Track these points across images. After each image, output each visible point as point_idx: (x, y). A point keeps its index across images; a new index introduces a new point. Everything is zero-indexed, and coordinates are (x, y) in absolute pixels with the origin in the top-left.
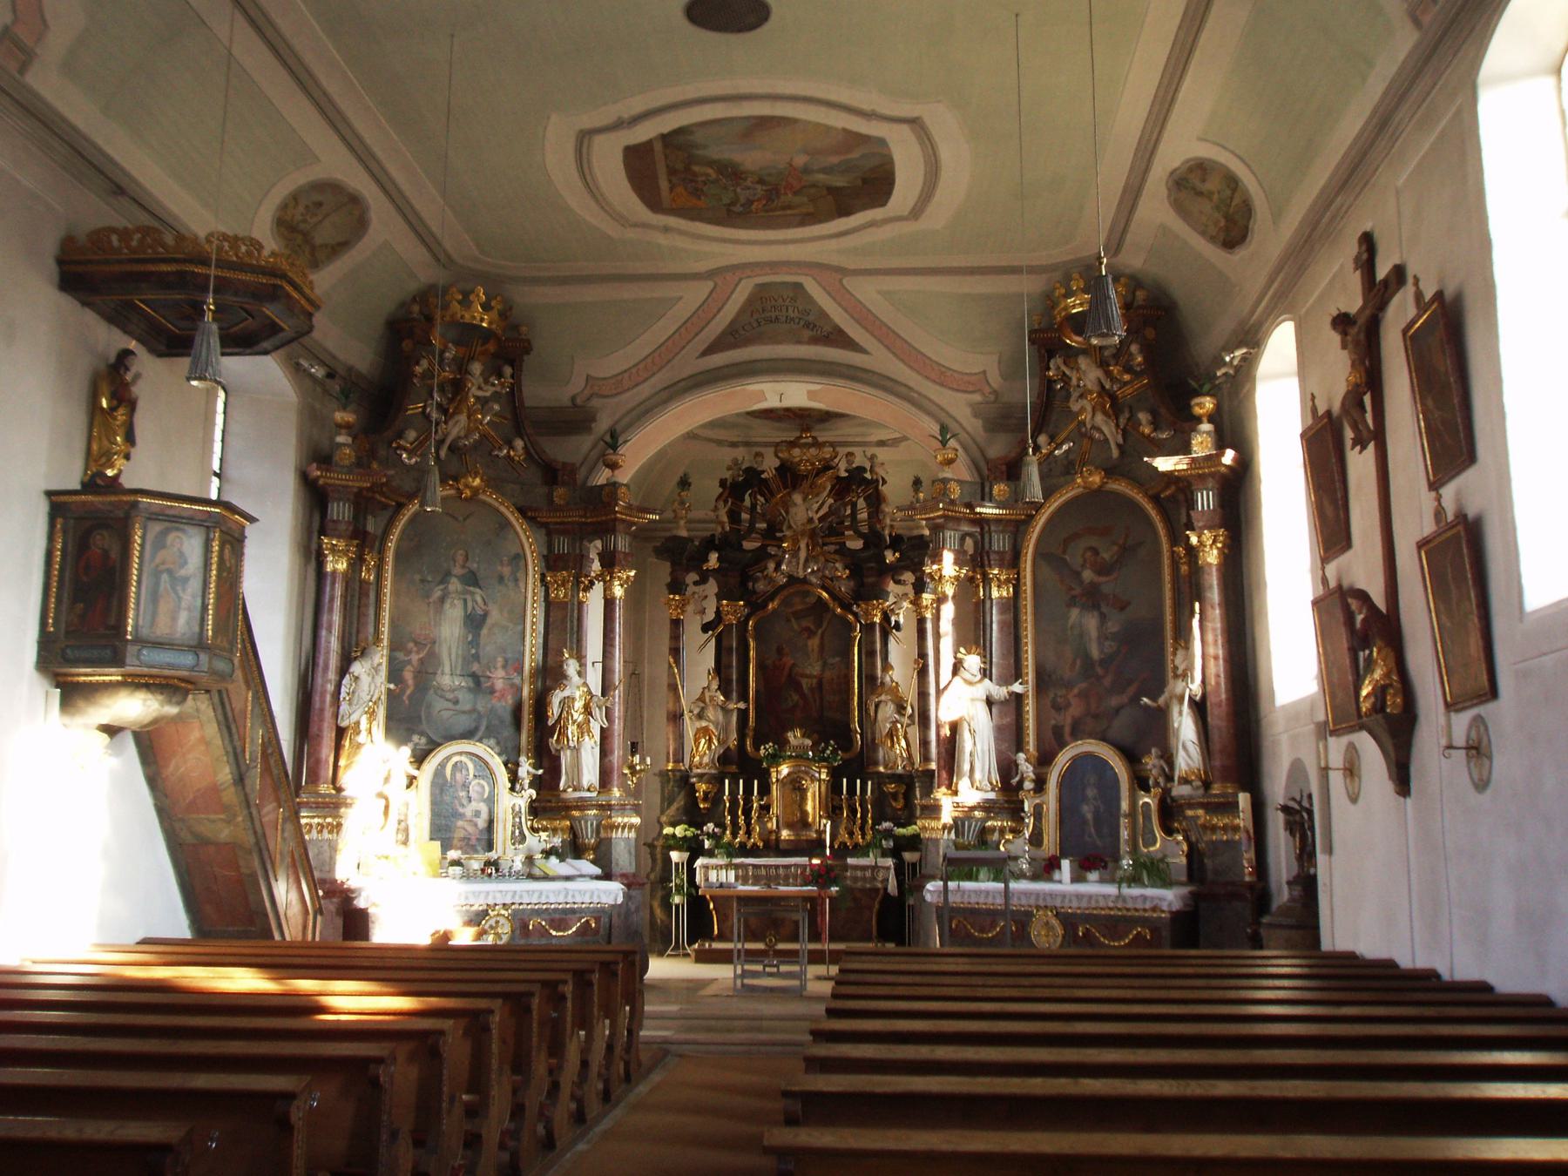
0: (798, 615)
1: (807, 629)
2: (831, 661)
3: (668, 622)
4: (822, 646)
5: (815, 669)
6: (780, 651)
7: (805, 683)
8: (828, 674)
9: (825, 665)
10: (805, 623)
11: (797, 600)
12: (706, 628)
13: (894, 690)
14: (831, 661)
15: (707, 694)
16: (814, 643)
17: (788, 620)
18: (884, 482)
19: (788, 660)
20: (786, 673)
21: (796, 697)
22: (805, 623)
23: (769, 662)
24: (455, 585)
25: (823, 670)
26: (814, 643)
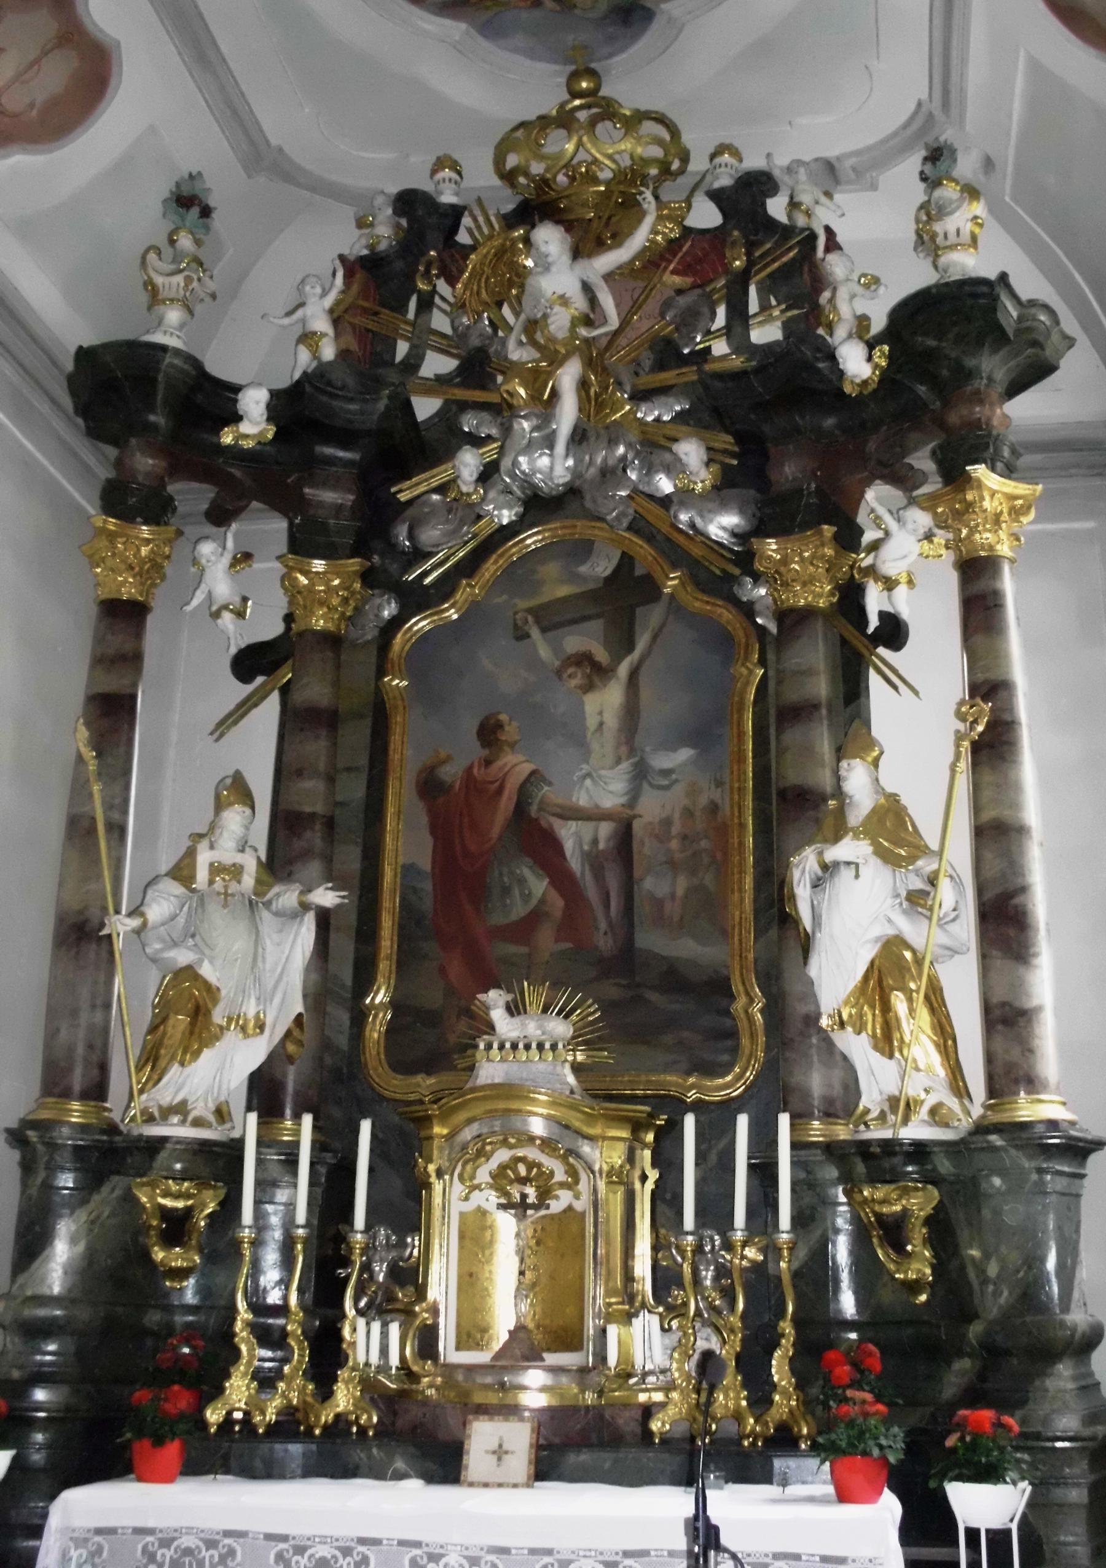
0: (551, 618)
1: (584, 659)
2: (663, 761)
3: (823, 1565)
4: (631, 712)
5: (608, 789)
6: (489, 733)
7: (572, 837)
8: (652, 807)
9: (641, 774)
10: (574, 642)
11: (551, 569)
12: (251, 662)
13: (892, 830)
14: (663, 761)
15: (204, 858)
16: (605, 703)
17: (522, 636)
18: (832, 245)
19: (516, 764)
20: (506, 804)
21: (539, 886)
22: (574, 642)
23: (451, 773)
24: (531, 1325)
25: (634, 796)
26: (605, 703)
